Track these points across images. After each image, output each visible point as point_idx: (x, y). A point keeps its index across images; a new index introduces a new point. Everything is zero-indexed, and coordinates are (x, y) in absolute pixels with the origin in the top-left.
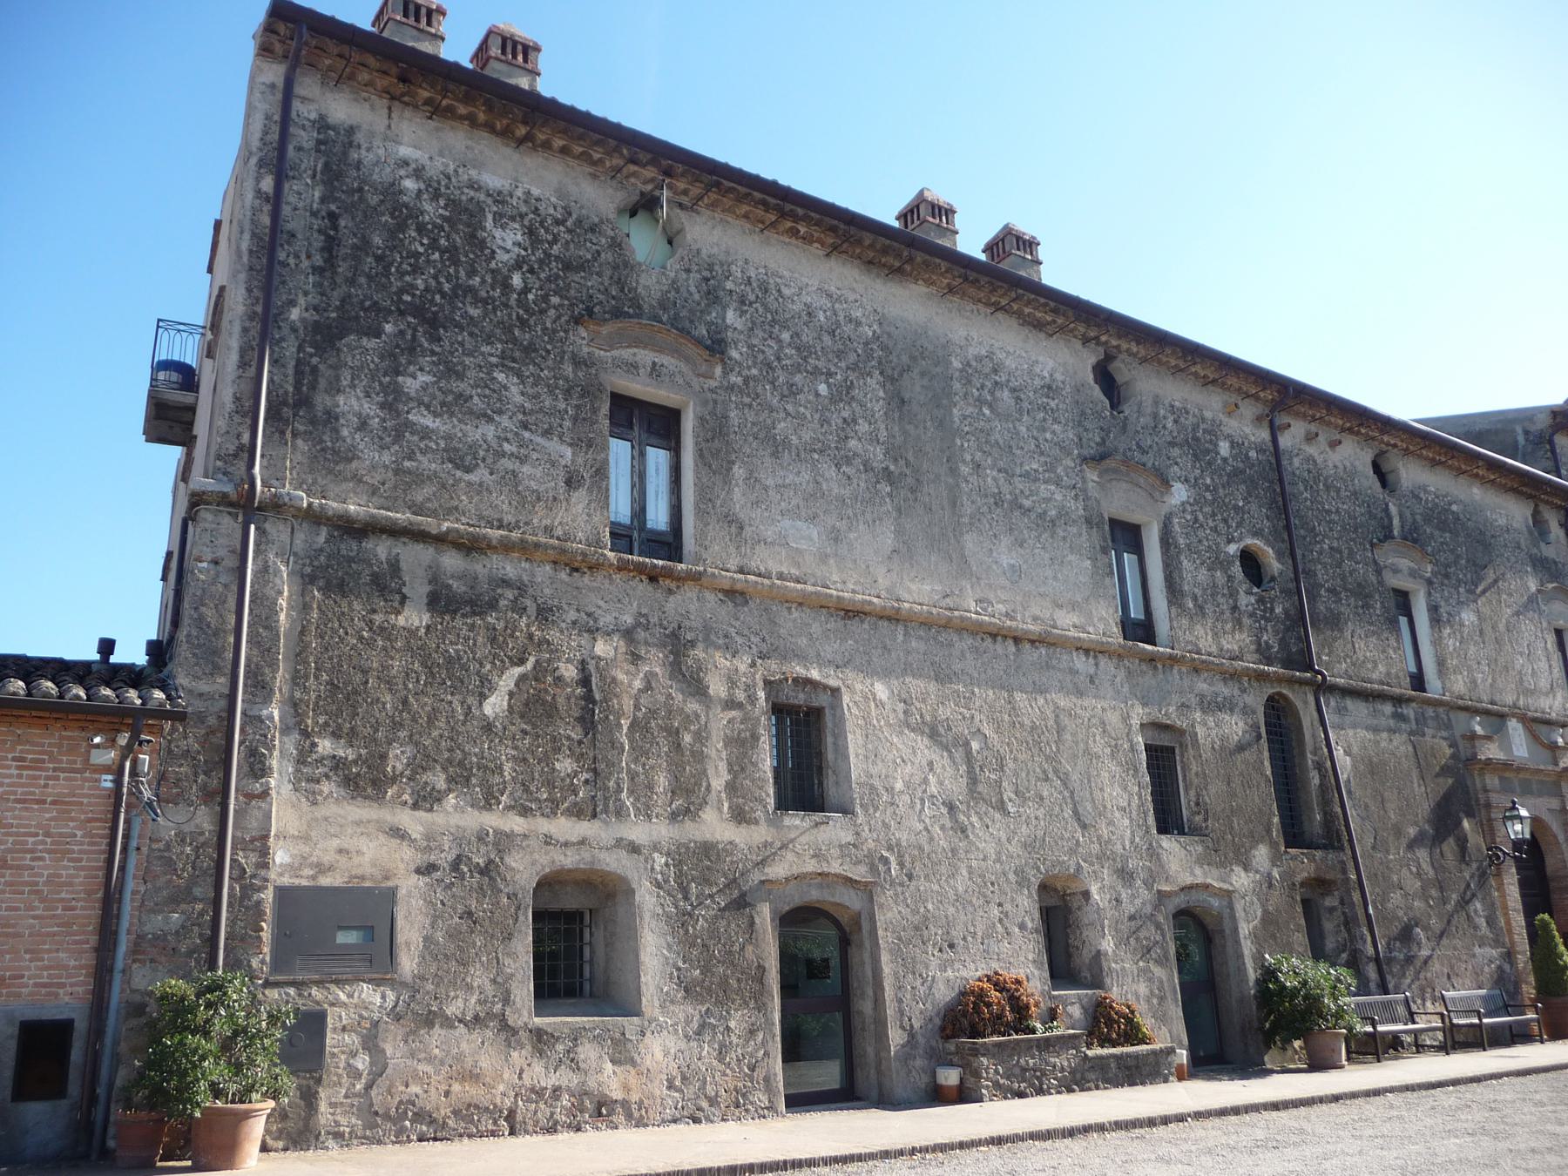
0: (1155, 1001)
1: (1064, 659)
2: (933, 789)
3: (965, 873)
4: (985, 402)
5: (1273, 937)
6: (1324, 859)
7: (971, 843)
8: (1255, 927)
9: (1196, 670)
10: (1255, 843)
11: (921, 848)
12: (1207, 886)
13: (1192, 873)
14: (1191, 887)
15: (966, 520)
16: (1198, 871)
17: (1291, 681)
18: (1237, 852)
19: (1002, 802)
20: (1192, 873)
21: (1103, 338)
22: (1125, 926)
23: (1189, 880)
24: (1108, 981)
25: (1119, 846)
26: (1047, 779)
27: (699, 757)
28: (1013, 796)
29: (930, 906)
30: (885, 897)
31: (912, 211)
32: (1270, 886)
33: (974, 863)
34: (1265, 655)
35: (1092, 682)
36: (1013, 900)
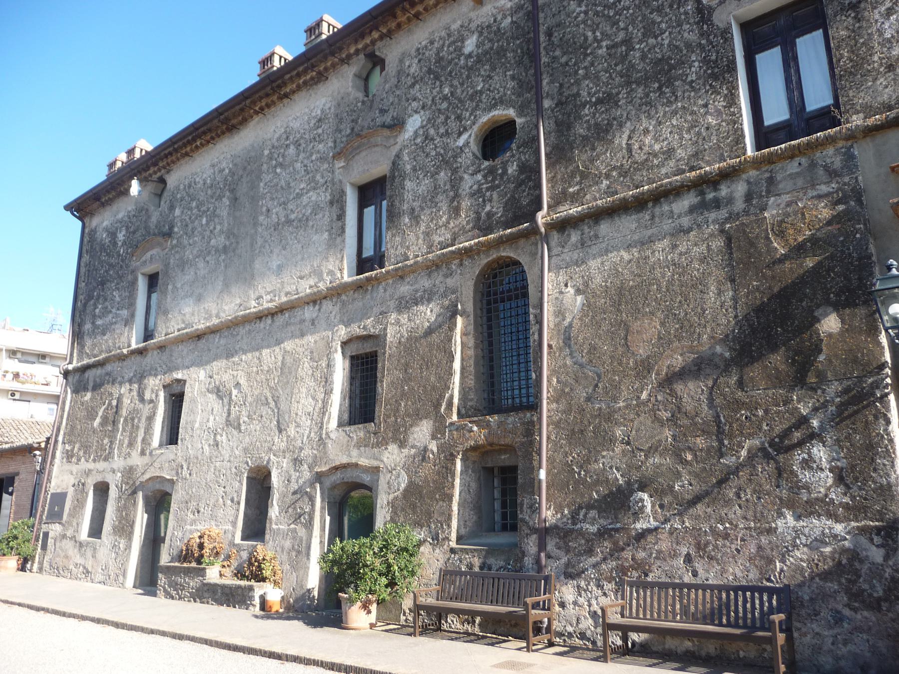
0: (294, 554)
1: (298, 313)
2: (210, 424)
3: (212, 470)
4: (234, 234)
5: (414, 507)
6: (500, 424)
7: (220, 452)
8: (396, 498)
9: (402, 277)
10: (417, 416)
11: (197, 458)
12: (356, 465)
13: (349, 456)
14: (344, 467)
15: (257, 252)
16: (355, 452)
17: (511, 240)
18: (396, 431)
19: (239, 424)
20: (349, 456)
21: (257, 108)
22: (290, 498)
23: (344, 460)
24: (267, 537)
25: (299, 442)
26: (268, 404)
27: (138, 427)
28: (246, 419)
29: (194, 490)
30: (179, 486)
31: (267, 59)
32: (424, 459)
33: (218, 464)
34: (483, 226)
35: (313, 324)
36: (231, 484)
